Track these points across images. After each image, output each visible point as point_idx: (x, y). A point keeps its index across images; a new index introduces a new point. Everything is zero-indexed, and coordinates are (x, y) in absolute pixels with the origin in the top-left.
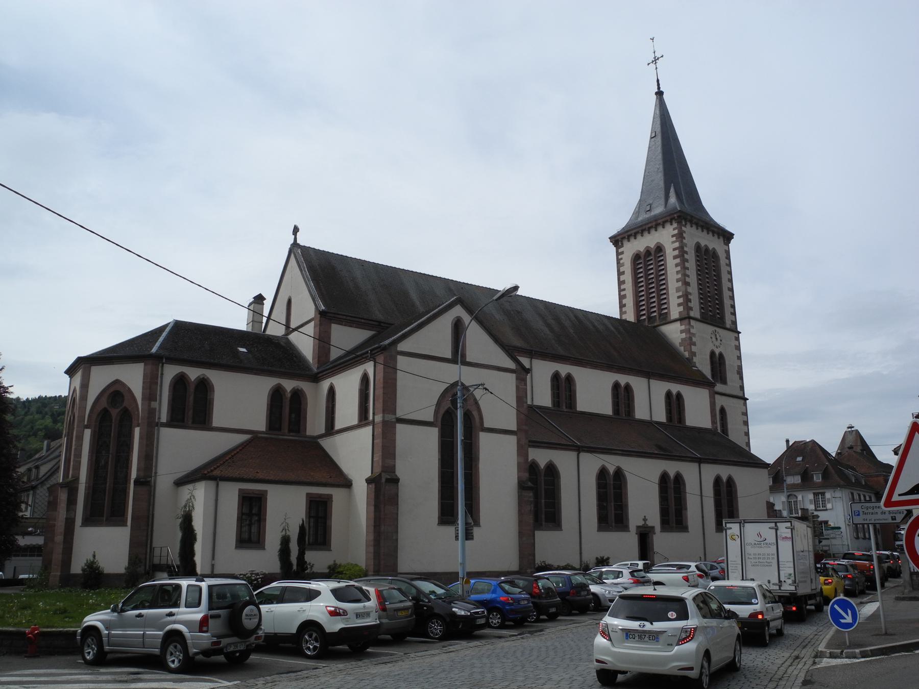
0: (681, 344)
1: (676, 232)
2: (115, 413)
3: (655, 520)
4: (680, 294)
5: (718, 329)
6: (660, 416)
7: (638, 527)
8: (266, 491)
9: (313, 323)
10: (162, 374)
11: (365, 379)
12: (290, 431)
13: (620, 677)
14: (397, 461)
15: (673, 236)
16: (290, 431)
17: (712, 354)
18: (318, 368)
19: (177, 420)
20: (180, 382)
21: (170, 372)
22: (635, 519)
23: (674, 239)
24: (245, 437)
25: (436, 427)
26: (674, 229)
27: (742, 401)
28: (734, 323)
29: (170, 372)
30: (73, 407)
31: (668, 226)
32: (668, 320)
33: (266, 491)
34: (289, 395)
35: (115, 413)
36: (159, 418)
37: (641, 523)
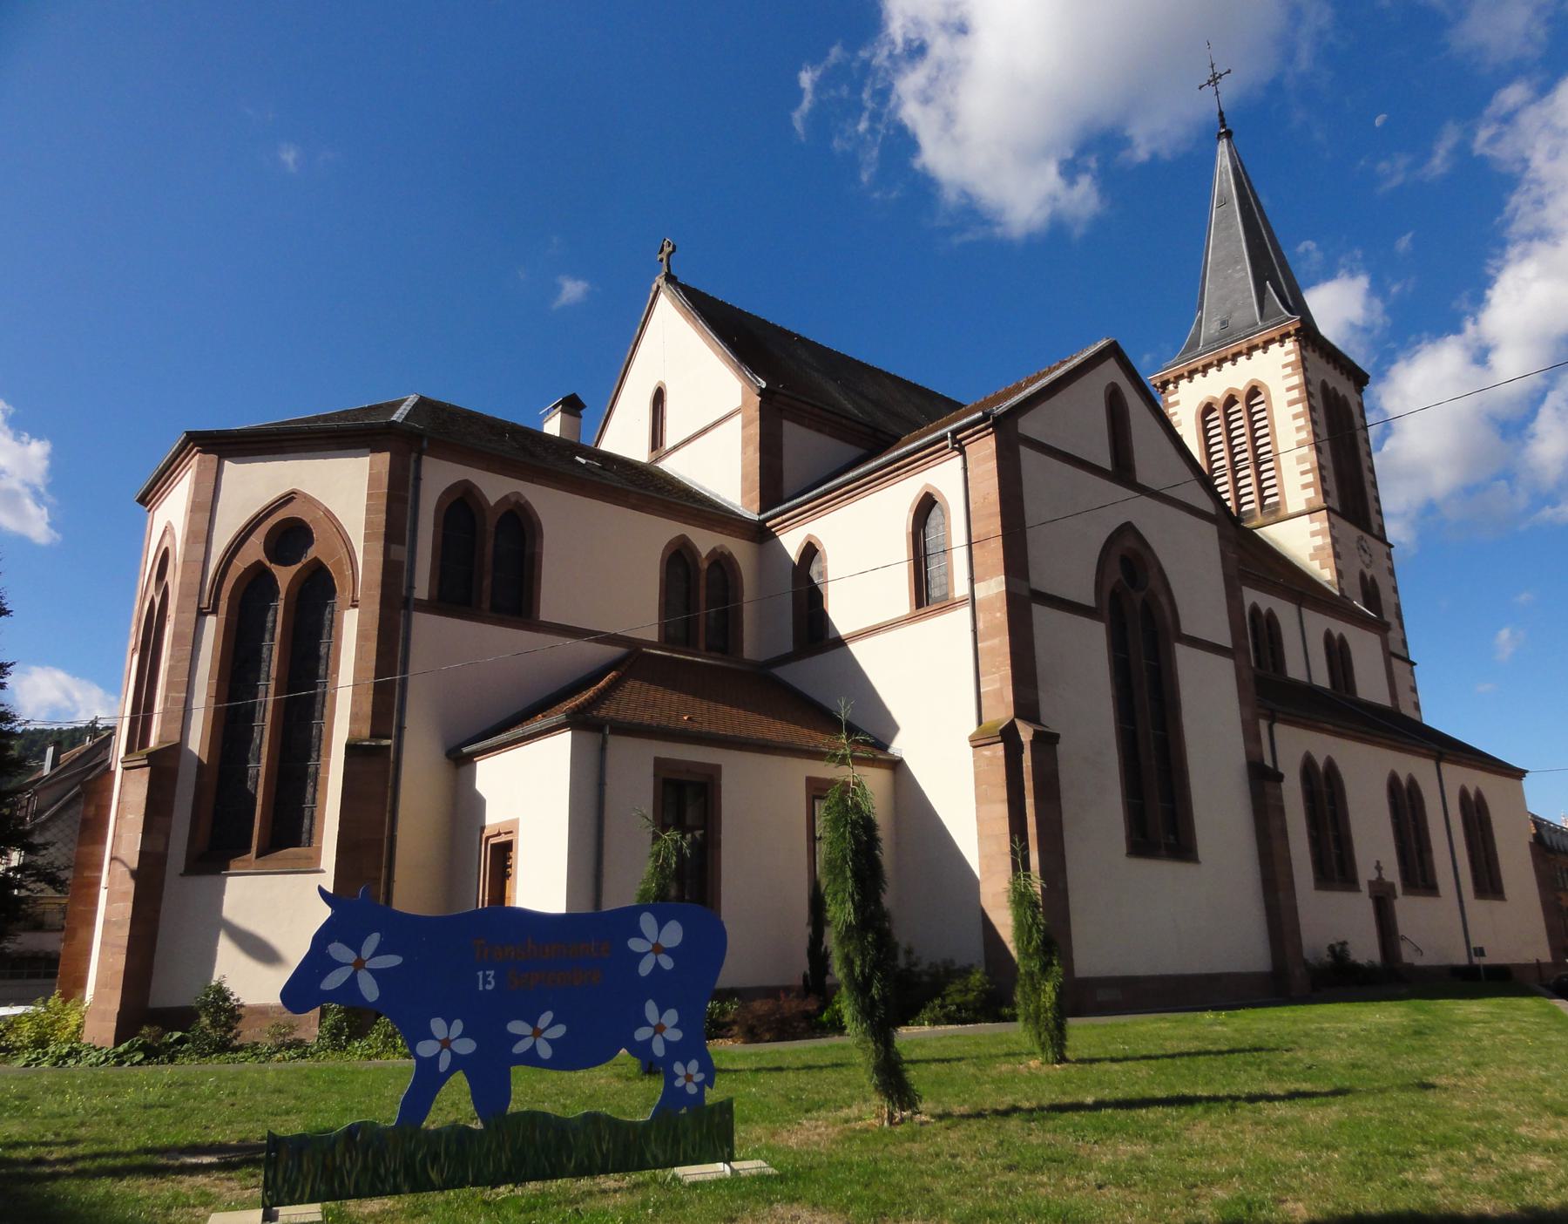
0: (1313, 557)
1: (1292, 358)
2: (284, 576)
3: (1392, 874)
4: (1307, 466)
5: (1366, 536)
6: (1322, 679)
7: (1371, 883)
8: (718, 768)
9: (738, 420)
10: (418, 478)
11: (927, 506)
12: (709, 648)
13: (139, 1057)
14: (1041, 694)
15: (1285, 366)
16: (709, 648)
17: (1363, 576)
18: (762, 511)
19: (455, 598)
20: (461, 507)
21: (439, 476)
22: (1365, 874)
23: (1289, 370)
24: (616, 651)
25: (1100, 619)
26: (1287, 354)
27: (1407, 666)
28: (1382, 528)
29: (439, 476)
30: (161, 574)
31: (1274, 347)
32: (1282, 514)
33: (718, 768)
34: (705, 565)
35: (284, 576)
36: (411, 587)
37: (1374, 877)
